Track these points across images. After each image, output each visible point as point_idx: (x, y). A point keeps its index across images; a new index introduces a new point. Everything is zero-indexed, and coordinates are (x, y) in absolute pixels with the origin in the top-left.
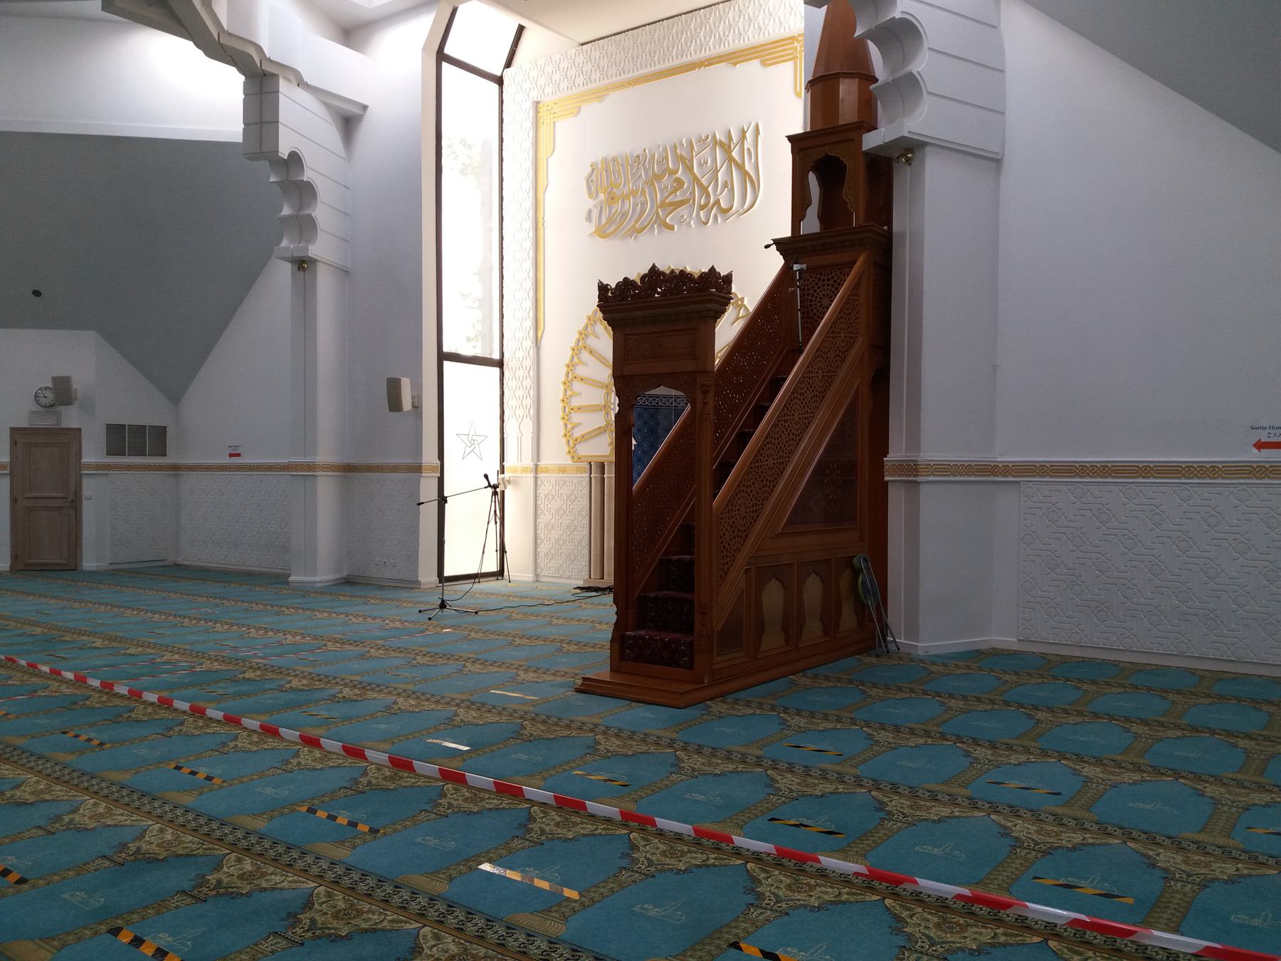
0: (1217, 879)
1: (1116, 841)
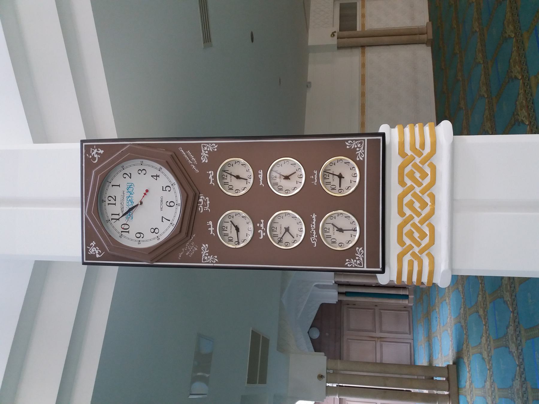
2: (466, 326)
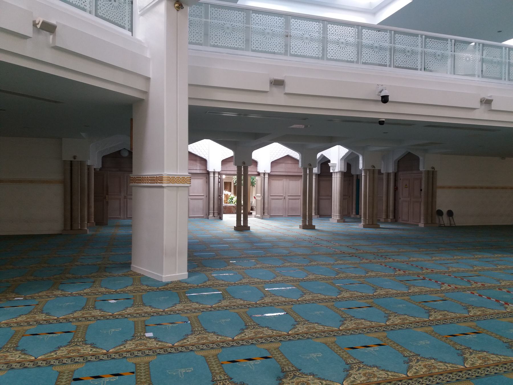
0: (131, 340)
1: (40, 358)
2: (167, 289)
